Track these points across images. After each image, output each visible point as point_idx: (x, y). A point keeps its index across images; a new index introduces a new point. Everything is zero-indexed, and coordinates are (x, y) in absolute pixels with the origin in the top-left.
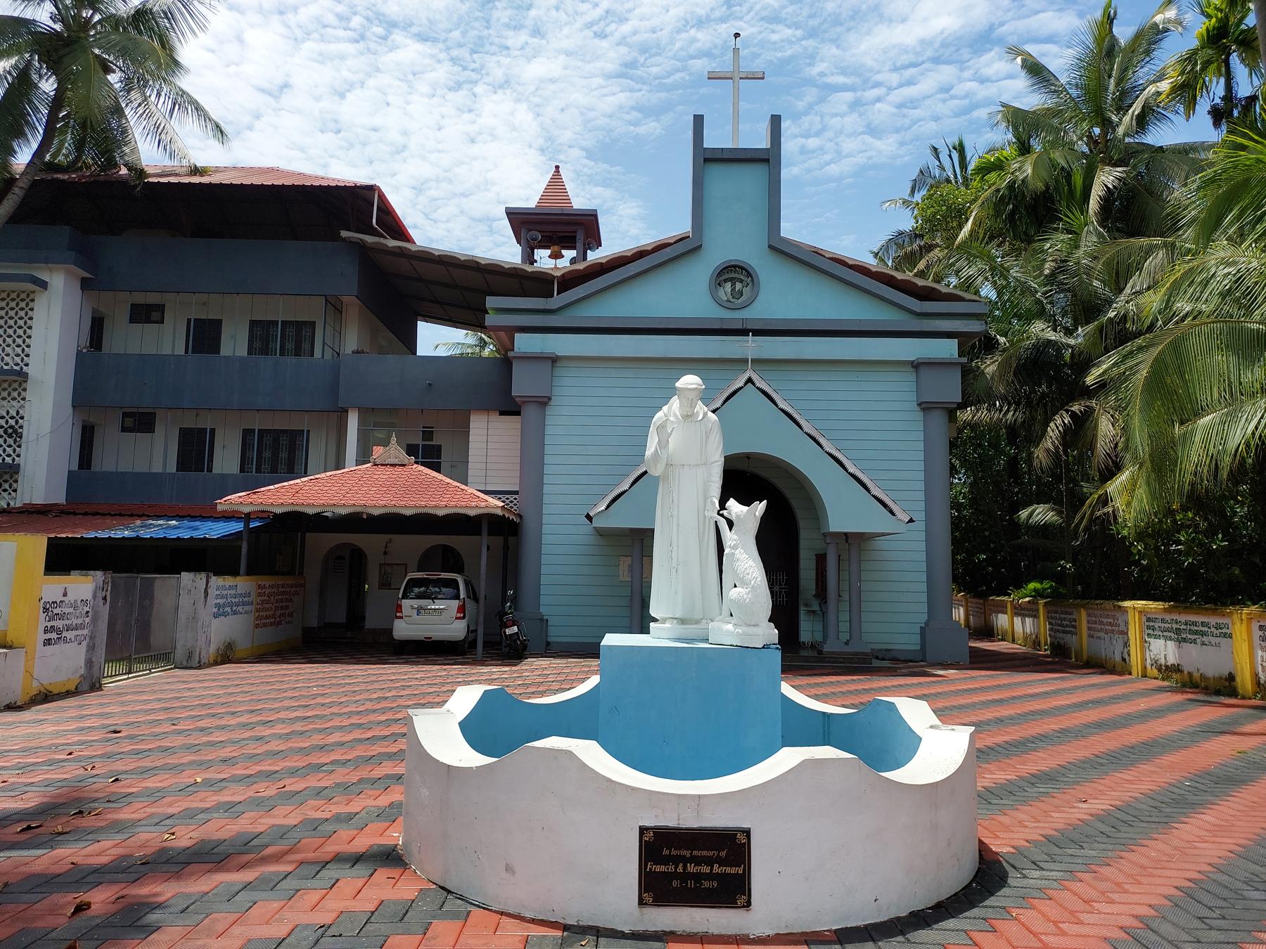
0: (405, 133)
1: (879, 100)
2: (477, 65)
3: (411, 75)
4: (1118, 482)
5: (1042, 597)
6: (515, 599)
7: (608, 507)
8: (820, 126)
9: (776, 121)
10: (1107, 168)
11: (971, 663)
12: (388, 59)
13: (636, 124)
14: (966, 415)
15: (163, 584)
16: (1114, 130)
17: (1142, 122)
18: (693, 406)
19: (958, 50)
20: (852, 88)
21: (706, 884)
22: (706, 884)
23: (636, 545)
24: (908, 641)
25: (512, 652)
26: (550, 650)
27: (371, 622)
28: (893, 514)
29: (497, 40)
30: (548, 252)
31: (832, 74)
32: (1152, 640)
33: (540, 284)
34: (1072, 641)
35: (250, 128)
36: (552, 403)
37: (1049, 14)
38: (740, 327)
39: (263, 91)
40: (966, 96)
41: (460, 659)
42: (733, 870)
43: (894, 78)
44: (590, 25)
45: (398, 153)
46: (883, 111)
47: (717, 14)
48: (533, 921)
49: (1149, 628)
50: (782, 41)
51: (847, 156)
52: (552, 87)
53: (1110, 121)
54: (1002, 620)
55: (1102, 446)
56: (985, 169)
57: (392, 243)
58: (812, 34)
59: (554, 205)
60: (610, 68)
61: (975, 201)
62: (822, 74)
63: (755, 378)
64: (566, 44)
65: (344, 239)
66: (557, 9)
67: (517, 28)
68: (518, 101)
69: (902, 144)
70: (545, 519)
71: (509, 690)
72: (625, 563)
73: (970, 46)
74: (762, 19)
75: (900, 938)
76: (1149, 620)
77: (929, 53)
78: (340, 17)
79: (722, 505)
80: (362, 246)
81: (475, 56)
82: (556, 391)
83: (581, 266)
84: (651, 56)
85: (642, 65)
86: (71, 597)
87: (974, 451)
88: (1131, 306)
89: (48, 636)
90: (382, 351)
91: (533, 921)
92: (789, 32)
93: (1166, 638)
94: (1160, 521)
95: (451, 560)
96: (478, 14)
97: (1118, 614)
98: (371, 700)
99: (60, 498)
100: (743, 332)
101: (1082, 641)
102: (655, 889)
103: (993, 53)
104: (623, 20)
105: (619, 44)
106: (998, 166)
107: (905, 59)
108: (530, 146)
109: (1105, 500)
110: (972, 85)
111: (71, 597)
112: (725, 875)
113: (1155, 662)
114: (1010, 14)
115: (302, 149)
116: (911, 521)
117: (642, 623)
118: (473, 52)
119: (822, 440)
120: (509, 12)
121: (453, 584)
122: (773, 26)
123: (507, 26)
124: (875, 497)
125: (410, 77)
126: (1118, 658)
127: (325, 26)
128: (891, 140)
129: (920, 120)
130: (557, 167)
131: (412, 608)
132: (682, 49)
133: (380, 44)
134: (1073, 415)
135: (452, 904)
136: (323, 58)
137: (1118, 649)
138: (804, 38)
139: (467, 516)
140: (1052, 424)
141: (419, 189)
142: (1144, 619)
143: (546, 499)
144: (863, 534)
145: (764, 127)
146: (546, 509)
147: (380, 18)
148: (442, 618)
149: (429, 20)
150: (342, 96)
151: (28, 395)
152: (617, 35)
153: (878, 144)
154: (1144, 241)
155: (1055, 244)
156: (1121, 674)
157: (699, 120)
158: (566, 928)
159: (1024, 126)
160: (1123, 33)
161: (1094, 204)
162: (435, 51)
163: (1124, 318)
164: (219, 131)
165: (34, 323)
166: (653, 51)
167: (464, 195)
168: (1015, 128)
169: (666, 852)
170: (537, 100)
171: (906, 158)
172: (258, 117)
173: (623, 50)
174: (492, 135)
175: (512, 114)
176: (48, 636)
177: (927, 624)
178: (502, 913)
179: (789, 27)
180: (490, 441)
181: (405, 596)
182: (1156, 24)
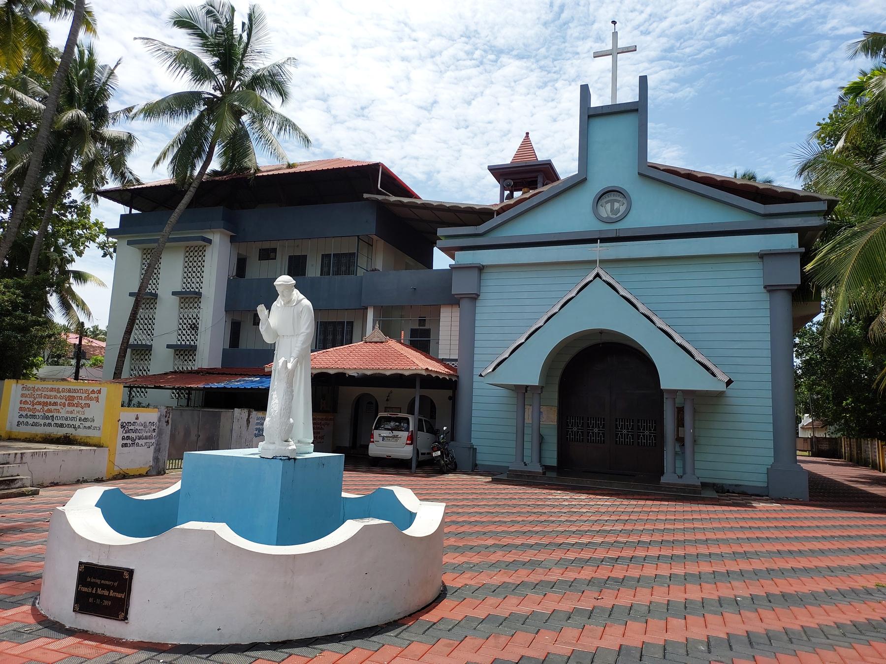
8: (833, 69)
11: (810, 500)
12: (498, 75)
13: (674, 91)
15: (225, 414)
21: (106, 603)
22: (106, 603)
24: (756, 478)
31: (844, 27)
35: (414, 133)
36: (480, 298)
38: (614, 235)
39: (421, 108)
42: (119, 595)
44: (637, 27)
45: (505, 136)
50: (797, 9)
59: (528, 160)
60: (653, 54)
62: (834, 29)
63: (602, 273)
65: (367, 199)
78: (467, 53)
80: (377, 201)
82: (483, 289)
85: (678, 49)
86: (141, 420)
89: (125, 442)
99: (218, 365)
100: (593, 241)
102: (84, 603)
104: (662, 19)
105: (659, 37)
111: (141, 420)
115: (445, 142)
118: (554, 60)
119: (654, 318)
123: (578, 38)
124: (698, 361)
125: (513, 84)
130: (527, 134)
132: (710, 31)
136: (457, 81)
139: (401, 375)
150: (469, 103)
151: (201, 305)
152: (658, 31)
164: (306, 140)
165: (205, 264)
169: (89, 580)
172: (418, 125)
173: (664, 40)
176: (125, 442)
181: (376, 428)
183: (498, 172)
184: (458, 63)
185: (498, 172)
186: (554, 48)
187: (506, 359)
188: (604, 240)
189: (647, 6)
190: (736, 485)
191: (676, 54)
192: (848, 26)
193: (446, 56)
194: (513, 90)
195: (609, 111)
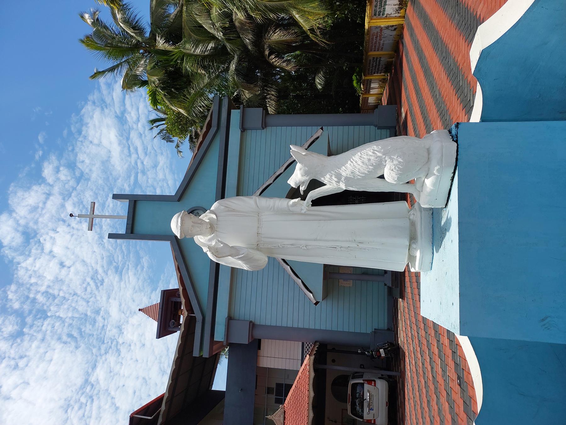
0: (138, 378)
1: (142, 163)
5: (361, 77)
6: (365, 348)
23: (334, 277)
25: (396, 355)
32: (386, 13)
33: (191, 321)
34: (384, 60)
36: (253, 320)
37: (114, 94)
40: (144, 127)
41: (400, 386)
43: (134, 156)
44: (97, 288)
46: (147, 162)
49: (379, 15)
51: (165, 176)
52: (123, 305)
54: (372, 100)
56: (155, 102)
57: (163, 407)
59: (158, 310)
60: (117, 278)
62: (129, 186)
64: (104, 299)
66: (88, 302)
67: (95, 321)
69: (162, 154)
70: (317, 327)
72: (342, 283)
73: (123, 125)
77: (125, 142)
81: (105, 342)
82: (247, 318)
84: (114, 260)
85: (117, 264)
88: (218, 25)
93: (385, 4)
95: (342, 381)
97: (372, 32)
103: (127, 116)
104: (96, 272)
105: (107, 274)
107: (126, 151)
109: (312, 30)
110: (140, 125)
113: (397, 11)
114: (112, 109)
118: (103, 343)
119: (277, 174)
120: (88, 325)
121: (354, 386)
122: (106, 206)
125: (112, 374)
126: (394, 33)
127: (84, 416)
128: (160, 159)
132: (112, 246)
133: (95, 388)
134: (270, 54)
136: (99, 418)
140: (275, 64)
142: (375, 17)
143: (306, 326)
145: (118, 202)
147: (83, 387)
148: (375, 393)
149: (86, 363)
150: (117, 408)
153: (161, 164)
155: (188, 66)
156: (401, 36)
159: (133, 82)
166: (112, 259)
168: (135, 84)
171: (168, 152)
173: (110, 272)
174: (142, 336)
175: (133, 325)
177: (376, 126)
183: (163, 332)
184: (86, 417)
185: (163, 332)
189: (85, 280)
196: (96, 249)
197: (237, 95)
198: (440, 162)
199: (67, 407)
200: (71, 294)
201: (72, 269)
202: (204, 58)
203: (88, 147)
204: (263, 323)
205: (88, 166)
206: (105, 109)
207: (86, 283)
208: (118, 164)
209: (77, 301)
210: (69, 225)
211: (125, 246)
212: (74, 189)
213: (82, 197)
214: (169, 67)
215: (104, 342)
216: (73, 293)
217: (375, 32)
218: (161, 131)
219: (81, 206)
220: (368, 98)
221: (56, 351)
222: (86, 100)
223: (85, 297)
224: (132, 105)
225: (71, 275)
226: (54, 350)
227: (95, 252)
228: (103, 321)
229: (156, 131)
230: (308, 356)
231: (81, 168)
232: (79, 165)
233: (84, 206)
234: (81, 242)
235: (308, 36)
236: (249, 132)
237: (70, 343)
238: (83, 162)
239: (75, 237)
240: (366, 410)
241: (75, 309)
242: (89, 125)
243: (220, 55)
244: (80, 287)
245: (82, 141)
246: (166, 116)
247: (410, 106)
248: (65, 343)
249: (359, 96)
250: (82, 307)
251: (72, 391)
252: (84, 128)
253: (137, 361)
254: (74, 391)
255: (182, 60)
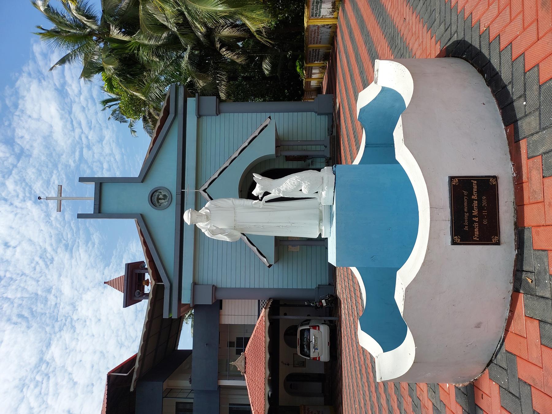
0: (95, 352)
1: (87, 137)
2: (64, 319)
3: (67, 350)
4: (251, 26)
6: (309, 301)
7: (264, 257)
8: (98, 163)
9: (82, 180)
10: (111, 33)
13: (94, 244)
14: (223, 96)
16: (94, 30)
17: (90, 17)
18: (202, 215)
19: (66, 103)
20: (81, 149)
21: (484, 203)
22: (484, 203)
23: (282, 244)
24: (322, 122)
25: (334, 303)
26: (332, 283)
27: (321, 371)
28: (267, 125)
29: (52, 309)
30: (146, 286)
31: (75, 157)
32: (322, 14)
33: (158, 290)
34: (322, 51)
36: (215, 285)
38: (180, 197)
40: (86, 100)
41: (338, 328)
43: (78, 131)
44: (47, 266)
45: (104, 355)
46: (92, 136)
47: (44, 208)
48: (512, 311)
50: (58, 179)
51: (112, 151)
53: (90, 32)
54: (314, 83)
55: (235, 33)
56: (111, 87)
57: (137, 365)
58: (55, 166)
59: (123, 283)
60: (67, 256)
61: (127, 92)
62: (74, 161)
63: (203, 188)
64: (55, 277)
65: (135, 389)
66: (38, 281)
67: (46, 300)
68: (81, 299)
69: (107, 128)
70: (271, 287)
71: (361, 314)
73: (64, 98)
74: (47, 188)
75: (509, 88)
76: (312, 16)
77: (67, 116)
78: (36, 386)
79: (256, 198)
80: (138, 380)
81: (59, 320)
82: (210, 282)
83: (150, 271)
84: (63, 238)
85: (67, 241)
87: (240, 95)
90: (190, 368)
91: (512, 311)
92: (54, 177)
93: (320, 8)
94: (269, 7)
95: (291, 331)
96: (38, 319)
97: (310, 30)
98: (361, 378)
100: (183, 194)
101: (322, 47)
102: (489, 235)
103: (68, 89)
104: (45, 251)
105: (57, 253)
106: (109, 81)
107: (69, 126)
108: (103, 293)
109: (259, 32)
110: (82, 98)
112: (478, 191)
113: (331, 13)
114: (51, 81)
116: (270, 118)
117: (322, 242)
118: (57, 320)
119: (233, 158)
120: (39, 304)
121: (303, 331)
122: (51, 183)
124: (259, 134)
125: (68, 351)
126: (329, 30)
127: (40, 393)
128: (106, 133)
129: (97, 120)
130: (105, 283)
131: (314, 352)
132: (60, 224)
133: (51, 366)
135: (501, 359)
136: (56, 394)
137: (324, 30)
138: (57, 170)
141: (121, 345)
142: (312, 18)
144: (276, 139)
146: (266, 286)
147: (37, 366)
148: (319, 336)
149: (40, 342)
150: (75, 383)
152: (52, 253)
153: (107, 138)
154: (141, 13)
155: (144, 56)
156: (335, 33)
157: (80, 216)
158: (516, 291)
159: (90, 70)
160: (51, 26)
161: (126, 38)
162: (56, 339)
163: (177, 24)
166: (61, 237)
167: (124, 323)
168: (92, 73)
170: (81, 290)
171: (114, 126)
173: (59, 250)
174: (97, 311)
175: (87, 301)
177: (316, 112)
178: (507, 331)
179: (52, 176)
180: (234, 314)
181: (309, 356)
182: (45, 10)
183: (129, 301)
184: (43, 394)
185: (129, 301)
186: (48, 321)
187: (256, 137)
188: (183, 187)
189: (33, 259)
190: (328, 130)
191: (70, 243)
192: (74, 155)
193: (34, 404)
194: (73, 351)
195: (98, 200)
196: (43, 227)
197: (191, 81)
198: (328, 185)
199: (22, 386)
200: (18, 274)
201: (18, 249)
202: (158, 47)
203: (26, 122)
204: (224, 286)
205: (28, 142)
206: (43, 81)
207: (35, 263)
208: (62, 140)
209: (25, 281)
210: (11, 204)
211: (74, 223)
212: (15, 166)
213: (24, 175)
214: (123, 55)
215: (57, 319)
216: (21, 274)
217: (313, 29)
218: (114, 112)
219: (24, 184)
220: (310, 82)
221: (6, 332)
222: (21, 72)
223: (34, 276)
224: (73, 77)
225: (18, 255)
226: (4, 331)
227: (42, 230)
228: (55, 299)
229: (109, 111)
230: (264, 309)
231: (21, 144)
232: (18, 141)
233: (27, 184)
234: (26, 221)
235: (255, 36)
236: (205, 118)
237: (21, 323)
238: (22, 137)
239: (18, 216)
240: (312, 350)
241: (23, 289)
242: (27, 98)
243: (173, 43)
244: (28, 266)
245: (19, 116)
246: (118, 97)
247: (342, 99)
248: (16, 323)
249: (302, 80)
250: (32, 286)
251: (27, 371)
252: (20, 102)
253: (93, 336)
254: (28, 370)
255: (139, 50)
